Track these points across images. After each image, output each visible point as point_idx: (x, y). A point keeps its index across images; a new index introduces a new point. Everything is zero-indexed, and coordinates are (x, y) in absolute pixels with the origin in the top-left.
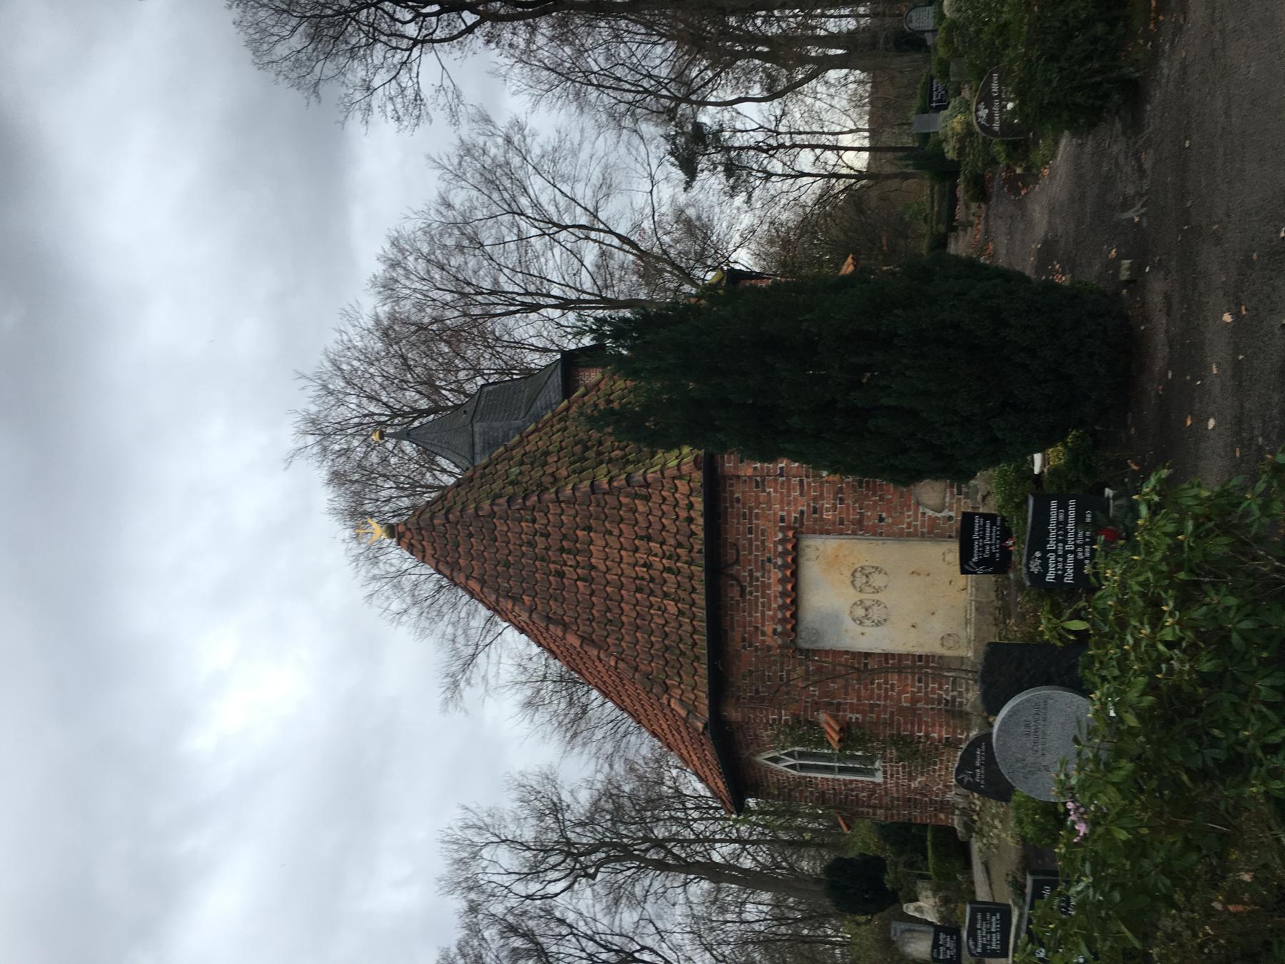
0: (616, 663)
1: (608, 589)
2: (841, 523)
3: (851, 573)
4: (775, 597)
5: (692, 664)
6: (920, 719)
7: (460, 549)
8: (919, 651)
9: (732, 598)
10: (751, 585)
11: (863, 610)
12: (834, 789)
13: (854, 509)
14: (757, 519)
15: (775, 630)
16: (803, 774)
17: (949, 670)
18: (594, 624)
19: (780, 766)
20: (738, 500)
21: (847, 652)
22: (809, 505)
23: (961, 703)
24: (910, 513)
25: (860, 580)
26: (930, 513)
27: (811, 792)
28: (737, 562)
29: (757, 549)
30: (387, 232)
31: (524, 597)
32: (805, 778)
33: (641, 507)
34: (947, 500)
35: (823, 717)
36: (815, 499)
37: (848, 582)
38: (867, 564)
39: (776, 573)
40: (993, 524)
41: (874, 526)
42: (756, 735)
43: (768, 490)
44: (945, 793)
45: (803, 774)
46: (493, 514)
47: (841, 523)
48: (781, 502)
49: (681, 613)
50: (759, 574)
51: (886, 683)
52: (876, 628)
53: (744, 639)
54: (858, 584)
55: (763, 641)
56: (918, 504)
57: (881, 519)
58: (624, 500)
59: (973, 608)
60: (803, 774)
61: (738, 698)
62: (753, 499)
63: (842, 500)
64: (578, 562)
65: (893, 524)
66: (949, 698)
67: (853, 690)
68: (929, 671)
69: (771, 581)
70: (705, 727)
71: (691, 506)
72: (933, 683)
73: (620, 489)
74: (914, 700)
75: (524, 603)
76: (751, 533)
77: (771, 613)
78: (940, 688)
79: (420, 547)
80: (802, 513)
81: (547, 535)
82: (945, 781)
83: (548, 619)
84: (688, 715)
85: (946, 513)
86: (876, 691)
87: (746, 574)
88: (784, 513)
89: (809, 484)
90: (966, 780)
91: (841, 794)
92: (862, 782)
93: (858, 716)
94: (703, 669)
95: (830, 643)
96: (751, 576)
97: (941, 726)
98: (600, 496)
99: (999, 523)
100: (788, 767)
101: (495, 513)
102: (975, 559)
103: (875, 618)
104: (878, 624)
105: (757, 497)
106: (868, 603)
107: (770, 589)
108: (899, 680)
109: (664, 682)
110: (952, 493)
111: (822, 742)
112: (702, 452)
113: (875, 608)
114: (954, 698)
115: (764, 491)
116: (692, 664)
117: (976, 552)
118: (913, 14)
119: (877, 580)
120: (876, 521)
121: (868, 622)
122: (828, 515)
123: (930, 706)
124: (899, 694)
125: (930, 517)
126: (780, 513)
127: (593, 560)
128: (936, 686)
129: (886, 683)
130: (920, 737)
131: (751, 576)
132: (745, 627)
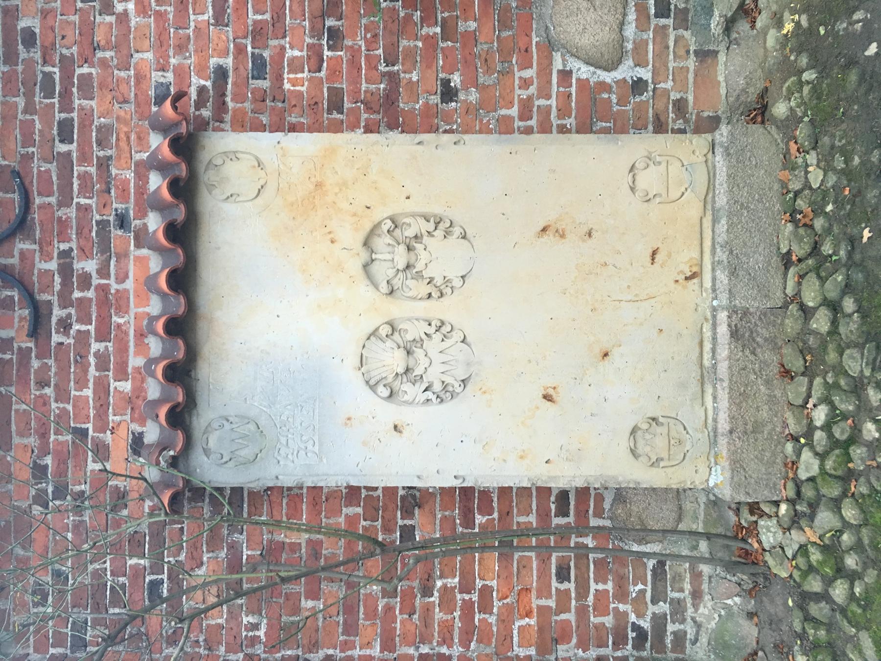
2: (336, 104)
3: (361, 237)
4: (140, 335)
10: (65, 301)
11: (401, 353)
13: (372, 64)
17: (644, 534)
20: (29, 38)
21: (353, 493)
22: (240, 50)
23: (679, 638)
24: (528, 73)
26: (583, 71)
34: (630, 31)
36: (259, 33)
37: (355, 265)
38: (410, 206)
39: (141, 261)
41: (429, 112)
43: (119, 7)
48: (161, 43)
50: (90, 266)
52: (435, 409)
53: (40, 471)
54: (382, 271)
56: (549, 46)
57: (448, 93)
59: (723, 330)
62: (73, 34)
63: (335, 36)
65: (481, 104)
66: (646, 624)
67: (371, 614)
68: (589, 541)
69: (129, 284)
72: (601, 578)
76: (66, 138)
77: (126, 386)
78: (622, 594)
80: (221, 73)
85: (626, 71)
86: (438, 615)
87: (53, 265)
88: (170, 76)
96: (66, 271)
103: (434, 376)
105: (87, 29)
106: (414, 331)
107: (123, 309)
108: (505, 576)
113: (434, 345)
114: (659, 622)
120: (435, 99)
121: (411, 391)
124: (506, 621)
125: (583, 84)
126: (156, 77)
128: (610, 586)
129: (466, 587)
131: (66, 271)
132: (44, 436)
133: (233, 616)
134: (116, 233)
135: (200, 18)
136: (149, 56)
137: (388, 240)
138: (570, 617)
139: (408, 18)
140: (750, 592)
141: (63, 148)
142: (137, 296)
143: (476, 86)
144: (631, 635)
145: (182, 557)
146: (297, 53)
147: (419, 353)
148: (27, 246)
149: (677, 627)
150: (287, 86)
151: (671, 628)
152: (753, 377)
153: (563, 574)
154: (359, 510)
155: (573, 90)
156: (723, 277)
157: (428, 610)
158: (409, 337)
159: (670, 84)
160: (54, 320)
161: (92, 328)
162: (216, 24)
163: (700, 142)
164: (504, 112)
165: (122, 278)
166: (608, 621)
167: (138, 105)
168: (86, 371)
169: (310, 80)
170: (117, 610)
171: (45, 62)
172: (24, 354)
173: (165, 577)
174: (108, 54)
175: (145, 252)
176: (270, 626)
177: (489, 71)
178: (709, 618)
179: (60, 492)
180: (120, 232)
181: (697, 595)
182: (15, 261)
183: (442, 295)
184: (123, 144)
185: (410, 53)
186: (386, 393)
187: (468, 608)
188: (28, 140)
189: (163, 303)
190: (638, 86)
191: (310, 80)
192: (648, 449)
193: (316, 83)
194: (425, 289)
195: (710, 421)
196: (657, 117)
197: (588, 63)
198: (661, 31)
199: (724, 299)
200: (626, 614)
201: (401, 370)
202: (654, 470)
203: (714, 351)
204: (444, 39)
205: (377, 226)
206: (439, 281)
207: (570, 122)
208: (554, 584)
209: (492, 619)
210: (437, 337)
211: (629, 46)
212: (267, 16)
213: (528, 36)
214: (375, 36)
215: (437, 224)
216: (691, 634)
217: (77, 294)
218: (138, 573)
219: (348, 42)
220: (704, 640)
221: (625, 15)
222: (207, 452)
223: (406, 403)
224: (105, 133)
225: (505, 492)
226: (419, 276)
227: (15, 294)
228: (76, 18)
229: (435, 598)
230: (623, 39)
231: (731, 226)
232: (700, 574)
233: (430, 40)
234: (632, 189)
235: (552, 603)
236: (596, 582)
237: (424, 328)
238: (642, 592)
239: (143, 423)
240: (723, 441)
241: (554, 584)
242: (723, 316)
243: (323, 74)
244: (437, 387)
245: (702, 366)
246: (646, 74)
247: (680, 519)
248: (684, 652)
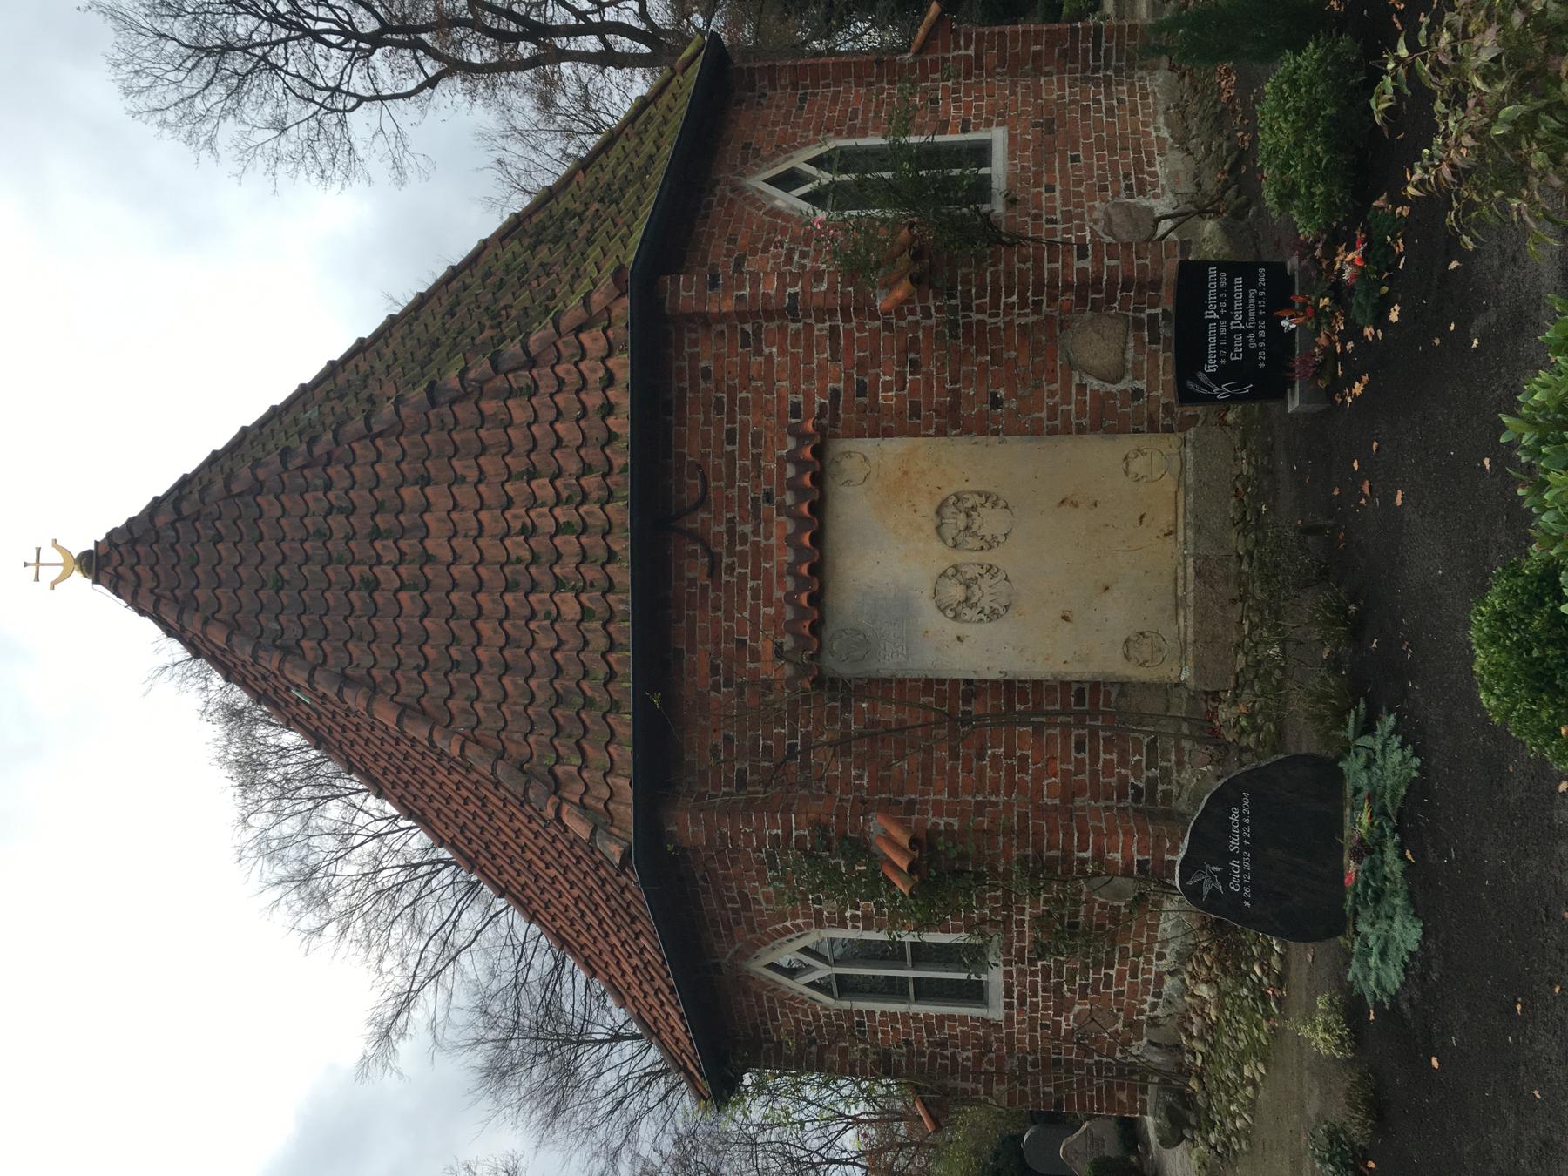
0: (462, 749)
1: (454, 596)
2: (915, 413)
4: (780, 576)
5: (604, 717)
6: (1082, 821)
7: (198, 570)
8: (1077, 671)
9: (692, 582)
10: (731, 552)
12: (908, 1043)
14: (745, 411)
15: (780, 646)
16: (846, 1004)
18: (425, 675)
20: (706, 374)
22: (849, 378)
23: (1167, 795)
24: (1054, 387)
26: (1094, 384)
27: (864, 1051)
28: (702, 502)
29: (744, 476)
31: (304, 644)
32: (849, 1013)
33: (520, 414)
34: (1130, 355)
35: (877, 825)
36: (862, 365)
37: (929, 528)
38: (968, 486)
40: (1250, 283)
42: (744, 897)
43: (766, 351)
44: (1128, 1042)
45: (846, 1004)
46: (258, 487)
47: (915, 413)
49: (586, 614)
51: (1009, 754)
52: (986, 626)
54: (949, 531)
55: (756, 672)
56: (1071, 366)
57: (996, 402)
58: (489, 406)
59: (1190, 570)
60: (845, 1004)
61: (701, 796)
64: (402, 554)
66: (1141, 785)
69: (773, 541)
70: (626, 856)
71: (610, 380)
73: (482, 383)
74: (1069, 792)
75: (304, 657)
76: (731, 441)
77: (771, 611)
78: (1123, 763)
79: (132, 578)
80: (835, 394)
81: (349, 512)
82: (1129, 1011)
83: (345, 680)
84: (593, 833)
85: (1126, 384)
86: (989, 773)
87: (722, 528)
88: (801, 397)
89: (849, 334)
90: (1206, 890)
91: (922, 1054)
92: (963, 1020)
93: (951, 820)
94: (624, 724)
95: (889, 663)
96: (731, 532)
97: (1128, 833)
98: (446, 409)
99: (1262, 281)
100: (812, 985)
101: (262, 484)
102: (1211, 367)
103: (986, 603)
104: (993, 615)
105: (745, 366)
106: (972, 572)
107: (769, 558)
109: (551, 771)
110: (1139, 341)
111: (875, 884)
113: (985, 583)
114: (1152, 783)
115: (759, 352)
116: (604, 717)
117: (1211, 349)
119: (990, 522)
121: (969, 613)
122: (887, 399)
123: (1101, 804)
124: (1038, 779)
126: (791, 397)
127: (428, 543)
128: (1115, 756)
129: (1009, 754)
130: (1083, 861)
131: (731, 532)
132: (717, 644)
133: (846, 768)
135: (821, 356)
136: (786, 383)
137: (953, 509)
138: (1085, 777)
139: (967, 350)
140: (1218, 761)
141: (729, 448)
142: (779, 548)
143: (1016, 397)
144: (1131, 791)
145: (810, 728)
146: (888, 378)
147: (975, 587)
148: (705, 515)
149: (1165, 787)
150: (881, 401)
151: (1160, 788)
152: (1211, 604)
153: (1080, 747)
154: (932, 699)
155: (1088, 398)
156: (1190, 534)
157: (981, 770)
158: (968, 576)
159: (1160, 392)
160: (723, 565)
161: (748, 571)
162: (832, 360)
163: (1174, 440)
164: (1036, 415)
165: (767, 538)
166: (1113, 781)
167: (779, 417)
168: (745, 600)
169: (897, 397)
170: (767, 764)
171: (717, 391)
172: (704, 589)
173: (799, 741)
174: (759, 383)
175: (784, 518)
176: (870, 776)
177: (1025, 386)
178: (1190, 781)
179: (728, 683)
180: (767, 505)
181: (1180, 763)
182: (697, 525)
183: (991, 547)
184: (769, 444)
186: (951, 614)
187: (1010, 769)
188: (706, 444)
189: (223, 449)
190: (1137, 394)
191: (897, 397)
192: (1137, 655)
193: (900, 398)
194: (978, 544)
195: (1182, 636)
196: (1150, 416)
197: (1098, 378)
199: (1191, 547)
200: (1127, 776)
201: (962, 599)
202: (1141, 669)
203: (1185, 584)
204: (992, 364)
205: (946, 500)
206: (988, 538)
207: (1085, 421)
208: (1074, 754)
209: (1028, 778)
210: (987, 576)
211: (1130, 365)
212: (867, 353)
213: (1055, 360)
214: (943, 364)
215: (987, 498)
216: (1175, 791)
217: (738, 548)
218: (780, 737)
219: (924, 369)
220: (1185, 796)
221: (1126, 343)
222: (832, 653)
223: (966, 621)
225: (1037, 684)
226: (975, 534)
227: (698, 548)
228: (737, 359)
229: (986, 762)
230: (1125, 360)
231: (1196, 497)
232: (1183, 749)
233: (983, 368)
234: (1126, 473)
235: (1071, 767)
236: (1105, 753)
237: (978, 570)
238: (1139, 761)
239: (783, 636)
240: (1190, 649)
241: (1074, 754)
242: (1190, 561)
243: (906, 392)
244: (987, 611)
245: (1176, 596)
247: (1168, 709)
248: (1170, 805)
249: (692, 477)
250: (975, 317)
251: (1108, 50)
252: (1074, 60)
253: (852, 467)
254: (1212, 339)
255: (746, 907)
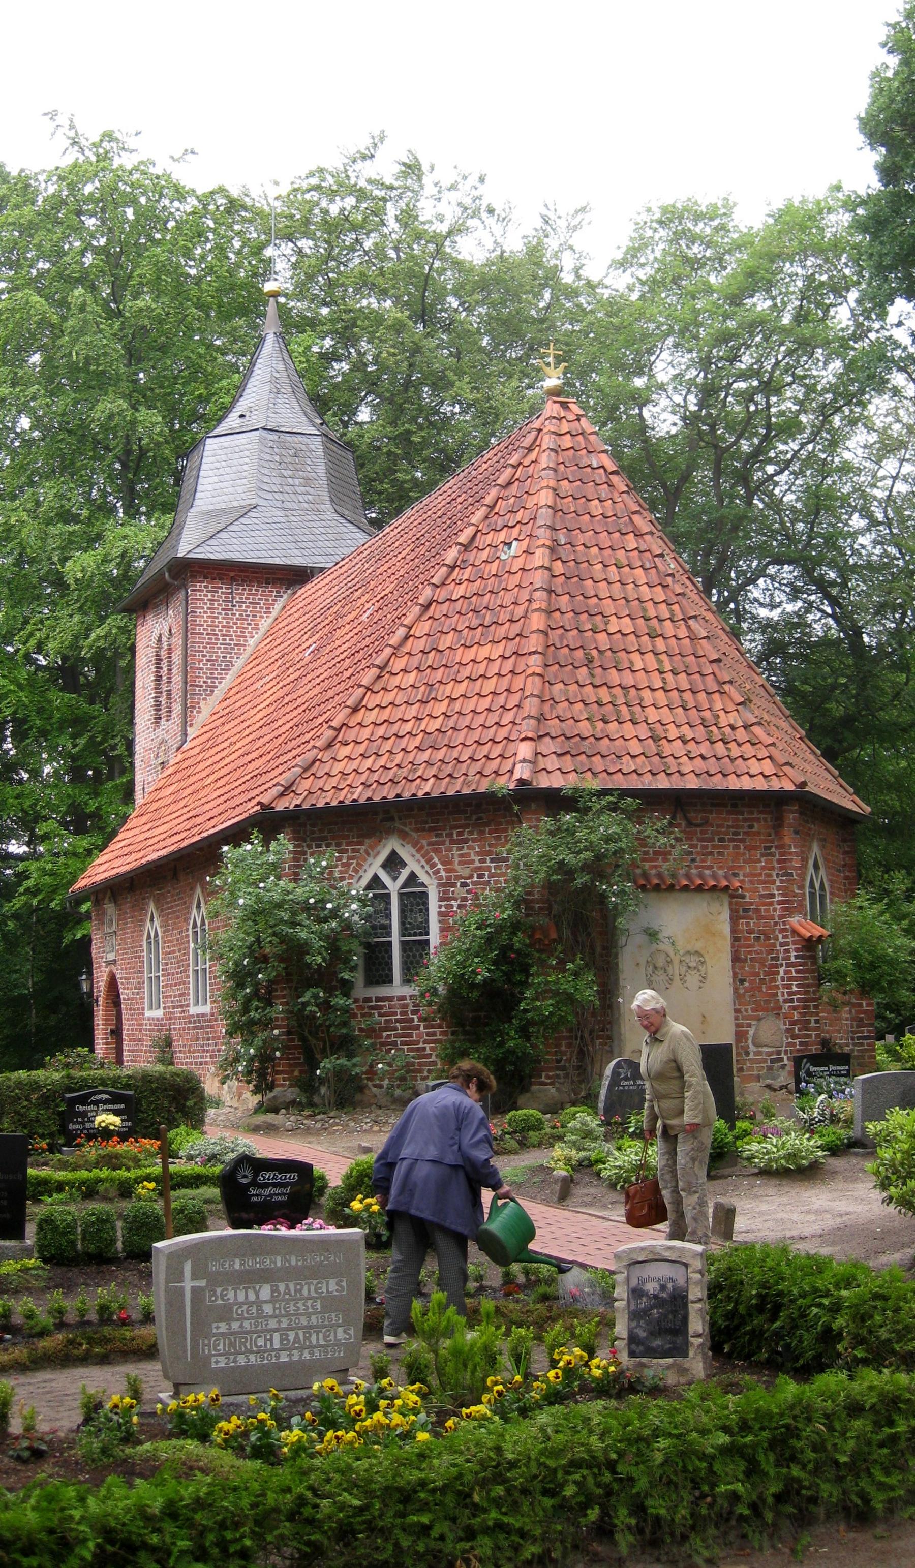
4: (656, 867)
13: (750, 953)
19: (194, 912)
20: (751, 827)
22: (751, 904)
24: (750, 1012)
25: (693, 961)
30: (566, 207)
36: (757, 911)
37: (689, 948)
48: (752, 875)
54: (687, 959)
56: (759, 1019)
80: (743, 897)
85: (752, 1048)
89: (771, 904)
102: (812, 1069)
105: (755, 848)
106: (670, 970)
112: (4, 846)
115: (762, 855)
118: (647, 1384)
120: (740, 977)
121: (650, 969)
126: (741, 873)
134: (689, 858)
185: (753, 967)
190: (747, 1054)
198: (765, 1061)
224: (720, 853)
233: (758, 974)
246: (751, 1056)
249: (702, 818)
250: (781, 970)
251: (862, 1044)
252: (858, 1026)
253: (715, 907)
254: (823, 1069)
255: (453, 842)
